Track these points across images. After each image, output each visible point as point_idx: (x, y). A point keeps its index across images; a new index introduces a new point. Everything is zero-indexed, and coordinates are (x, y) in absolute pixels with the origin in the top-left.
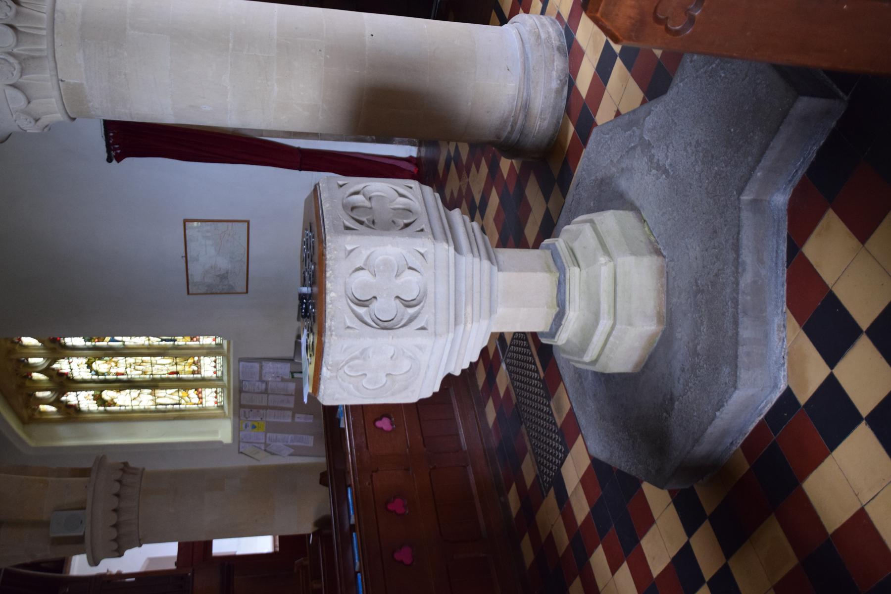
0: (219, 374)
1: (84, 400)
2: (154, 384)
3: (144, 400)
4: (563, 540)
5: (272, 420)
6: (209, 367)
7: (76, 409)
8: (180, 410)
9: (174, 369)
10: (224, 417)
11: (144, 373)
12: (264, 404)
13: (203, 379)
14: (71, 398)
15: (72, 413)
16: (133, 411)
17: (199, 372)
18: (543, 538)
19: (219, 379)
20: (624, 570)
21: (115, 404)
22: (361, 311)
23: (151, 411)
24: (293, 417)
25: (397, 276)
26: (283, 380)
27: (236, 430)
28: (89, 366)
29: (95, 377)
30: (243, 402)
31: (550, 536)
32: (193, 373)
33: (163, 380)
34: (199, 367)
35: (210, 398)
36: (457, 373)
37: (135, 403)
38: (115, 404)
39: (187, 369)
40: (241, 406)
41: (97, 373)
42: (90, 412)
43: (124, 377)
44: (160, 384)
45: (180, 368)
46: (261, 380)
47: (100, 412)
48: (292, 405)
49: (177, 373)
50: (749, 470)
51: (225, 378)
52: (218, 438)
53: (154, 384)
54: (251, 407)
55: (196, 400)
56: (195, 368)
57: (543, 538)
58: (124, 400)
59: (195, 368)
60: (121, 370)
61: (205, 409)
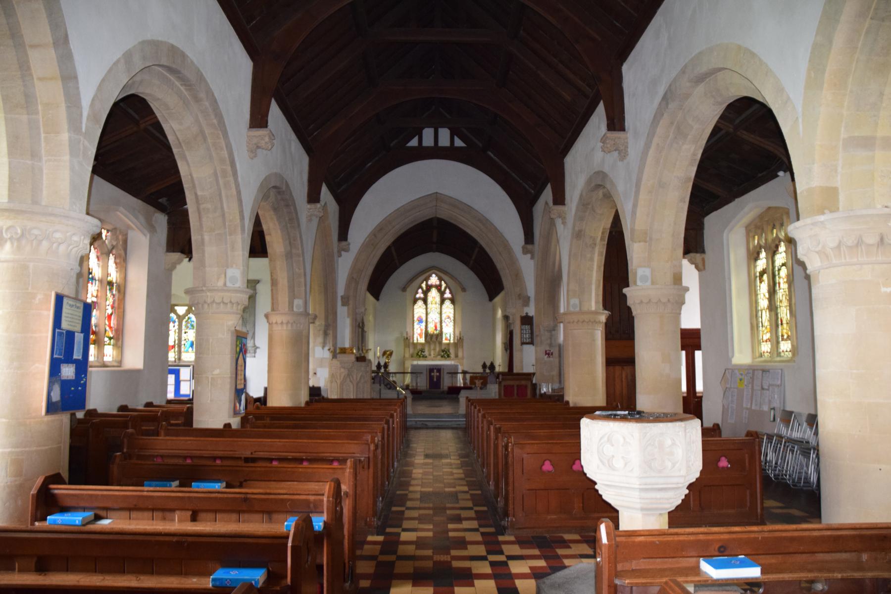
0: (782, 354)
1: (761, 264)
2: (773, 307)
3: (763, 303)
4: (560, 552)
5: (745, 393)
6: (785, 346)
7: (757, 258)
8: (758, 327)
9: (784, 322)
10: (754, 358)
11: (781, 301)
12: (755, 388)
13: (778, 343)
14: (763, 255)
15: (754, 257)
16: (756, 295)
17: (783, 340)
18: (571, 545)
19: (779, 354)
20: (528, 571)
21: (761, 282)
22: (606, 439)
23: (756, 307)
24: (747, 409)
25: (623, 457)
26: (770, 401)
27: (740, 368)
28: (783, 265)
29: (777, 269)
30: (756, 372)
31: (569, 547)
32: (782, 336)
33: (777, 314)
34: (786, 340)
35: (766, 347)
36: (596, 487)
37: (762, 296)
38: (761, 282)
39: (785, 331)
40: (754, 370)
41: (779, 270)
42: (755, 267)
43: (777, 288)
44: (773, 313)
45: (785, 326)
46: (770, 385)
47: (755, 274)
48: (753, 408)
49: (782, 324)
50: (496, 583)
51: (778, 359)
52: (736, 354)
53: (773, 307)
54: (752, 378)
55: (765, 339)
56: (785, 337)
57: (571, 545)
58: (763, 289)
59: (785, 337)
60: (782, 286)
61: (759, 344)
